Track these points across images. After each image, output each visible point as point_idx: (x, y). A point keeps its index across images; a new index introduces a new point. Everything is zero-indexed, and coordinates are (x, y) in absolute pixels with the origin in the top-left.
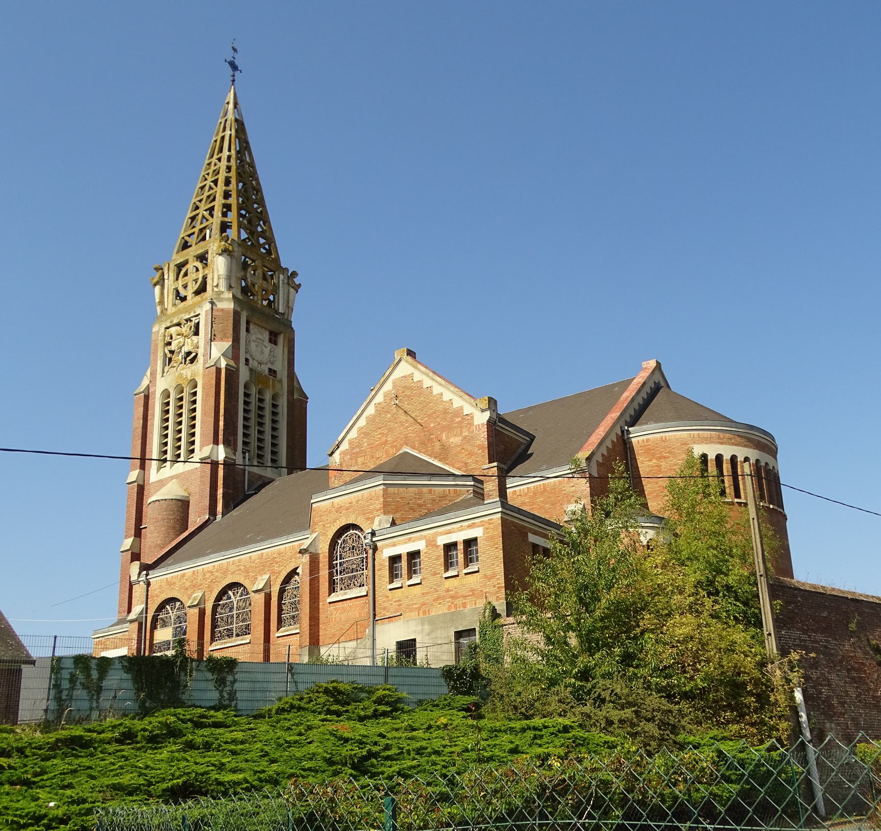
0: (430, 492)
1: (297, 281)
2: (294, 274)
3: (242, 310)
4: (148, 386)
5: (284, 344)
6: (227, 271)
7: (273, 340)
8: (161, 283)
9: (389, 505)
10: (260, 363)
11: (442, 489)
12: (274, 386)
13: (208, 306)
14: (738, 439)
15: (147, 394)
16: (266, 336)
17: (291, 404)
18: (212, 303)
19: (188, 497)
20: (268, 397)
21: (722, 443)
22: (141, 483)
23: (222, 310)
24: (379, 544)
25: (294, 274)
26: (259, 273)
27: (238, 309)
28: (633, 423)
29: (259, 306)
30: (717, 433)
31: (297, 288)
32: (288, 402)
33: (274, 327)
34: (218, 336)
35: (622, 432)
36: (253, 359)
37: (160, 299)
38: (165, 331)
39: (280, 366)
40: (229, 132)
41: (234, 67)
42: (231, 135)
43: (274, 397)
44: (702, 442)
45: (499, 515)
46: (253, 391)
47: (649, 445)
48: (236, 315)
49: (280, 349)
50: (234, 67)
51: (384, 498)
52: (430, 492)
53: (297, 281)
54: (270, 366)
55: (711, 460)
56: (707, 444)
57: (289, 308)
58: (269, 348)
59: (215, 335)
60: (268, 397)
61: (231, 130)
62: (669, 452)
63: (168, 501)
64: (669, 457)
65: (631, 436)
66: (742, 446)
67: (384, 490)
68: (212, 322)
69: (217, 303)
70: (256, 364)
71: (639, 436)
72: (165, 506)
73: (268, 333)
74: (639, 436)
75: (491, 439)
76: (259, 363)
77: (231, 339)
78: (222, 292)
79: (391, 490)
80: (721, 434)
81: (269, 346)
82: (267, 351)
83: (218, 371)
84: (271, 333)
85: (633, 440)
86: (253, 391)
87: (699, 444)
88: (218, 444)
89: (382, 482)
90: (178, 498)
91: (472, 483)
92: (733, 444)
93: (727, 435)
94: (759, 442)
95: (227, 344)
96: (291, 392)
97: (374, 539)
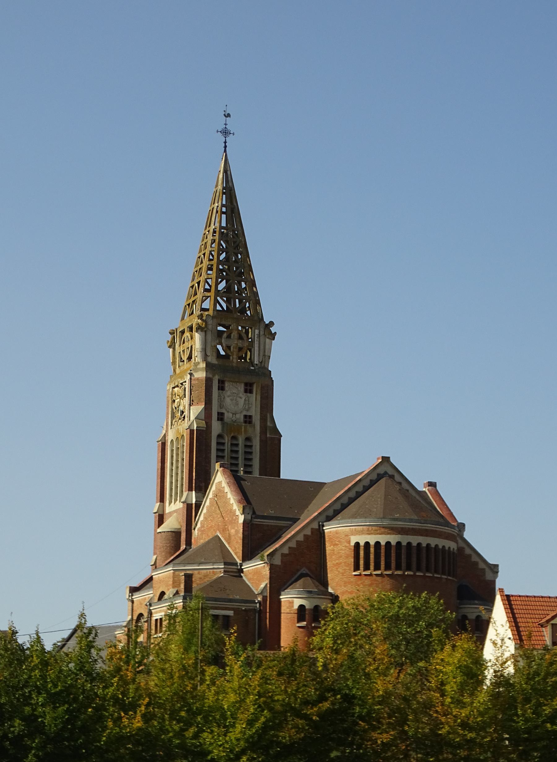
0: (199, 573)
1: (273, 330)
2: (272, 323)
3: (214, 376)
4: (165, 435)
5: (256, 391)
6: (202, 345)
7: (248, 389)
8: (173, 347)
9: (176, 582)
10: (234, 414)
11: (205, 571)
12: (246, 431)
13: (189, 376)
14: (383, 530)
15: (163, 441)
16: (242, 388)
17: (264, 442)
18: (191, 374)
19: (180, 529)
20: (241, 441)
21: (369, 534)
22: (161, 513)
23: (198, 379)
24: (153, 611)
25: (272, 323)
26: (234, 335)
27: (211, 376)
28: (329, 519)
29: (234, 365)
30: (368, 527)
31: (273, 336)
32: (261, 441)
33: (248, 379)
34: (195, 401)
35: (319, 525)
36: (228, 412)
37: (173, 360)
38: (172, 390)
39: (255, 413)
40: (217, 204)
41: (226, 132)
42: (218, 207)
43: (248, 439)
44: (357, 534)
45: (182, 604)
46: (227, 440)
47: (331, 535)
48: (208, 381)
49: (255, 398)
50: (226, 132)
51: (173, 578)
52: (199, 573)
53: (273, 330)
54: (245, 413)
55: (362, 546)
56: (360, 535)
57: (266, 357)
58: (243, 399)
59: (193, 401)
60: (241, 441)
61: (218, 203)
62: (339, 541)
63: (166, 533)
64: (338, 545)
65: (324, 528)
66: (385, 534)
67: (174, 573)
68: (191, 390)
69: (194, 374)
70: (231, 415)
71: (329, 529)
72: (164, 537)
73: (243, 385)
74: (329, 529)
75: (246, 533)
76: (233, 414)
77: (204, 403)
78: (199, 363)
79: (177, 573)
80: (370, 528)
81: (243, 396)
82: (241, 402)
83: (192, 432)
84: (246, 384)
85: (326, 531)
86: (227, 440)
87: (355, 535)
88: (192, 491)
89: (171, 569)
90: (176, 530)
91: (223, 567)
92: (377, 534)
93: (374, 528)
94: (402, 528)
95: (201, 407)
96: (264, 429)
97: (151, 608)
